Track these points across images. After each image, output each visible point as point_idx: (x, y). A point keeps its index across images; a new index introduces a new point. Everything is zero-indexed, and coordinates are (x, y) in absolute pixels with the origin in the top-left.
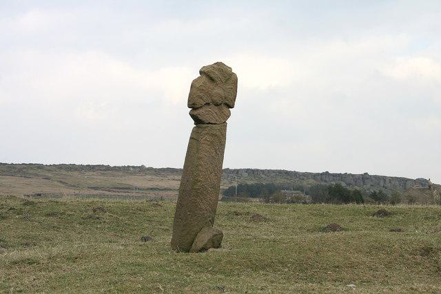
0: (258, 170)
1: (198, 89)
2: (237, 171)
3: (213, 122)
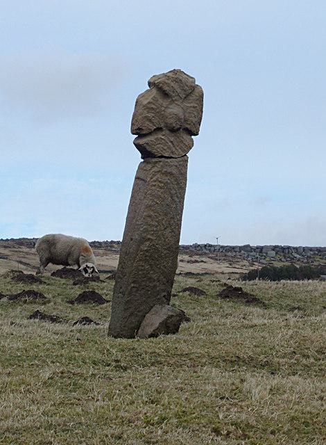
0: (289, 248)
1: (146, 107)
2: (260, 249)
3: (166, 155)
